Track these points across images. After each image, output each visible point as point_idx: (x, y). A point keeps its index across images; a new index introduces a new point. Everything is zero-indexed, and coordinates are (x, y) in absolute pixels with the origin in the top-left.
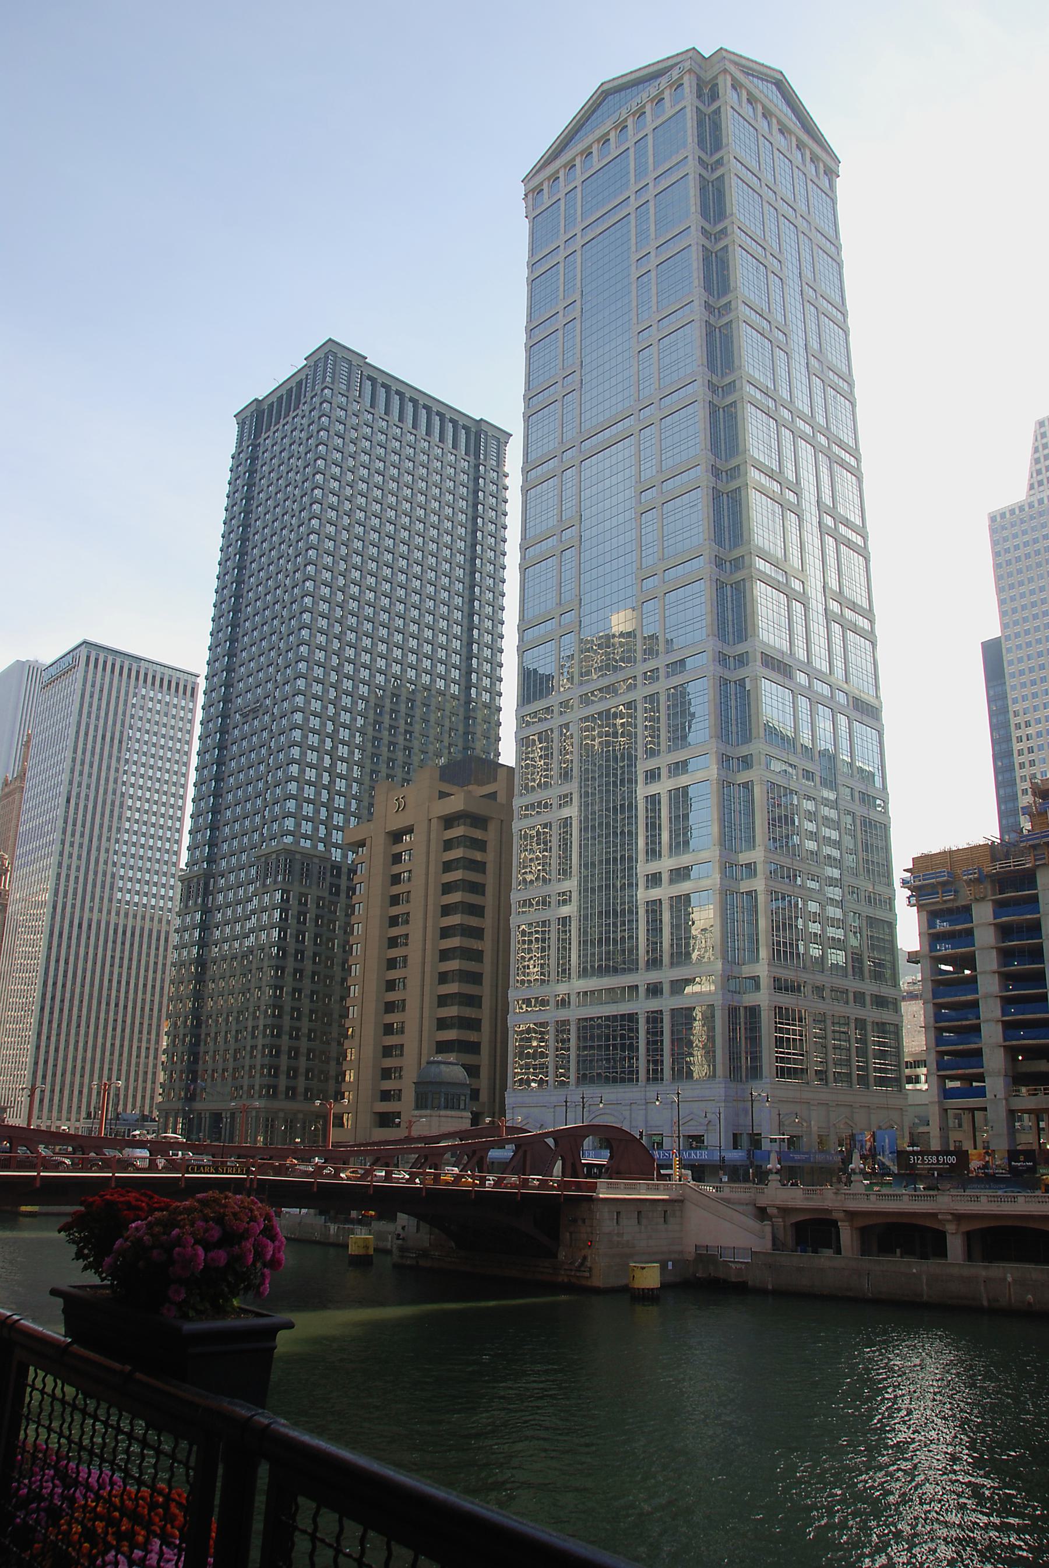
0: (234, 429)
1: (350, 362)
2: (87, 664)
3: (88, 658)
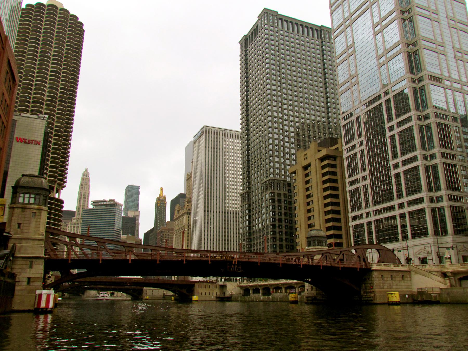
0: (239, 47)
1: (272, 15)
2: (206, 133)
3: (206, 131)
